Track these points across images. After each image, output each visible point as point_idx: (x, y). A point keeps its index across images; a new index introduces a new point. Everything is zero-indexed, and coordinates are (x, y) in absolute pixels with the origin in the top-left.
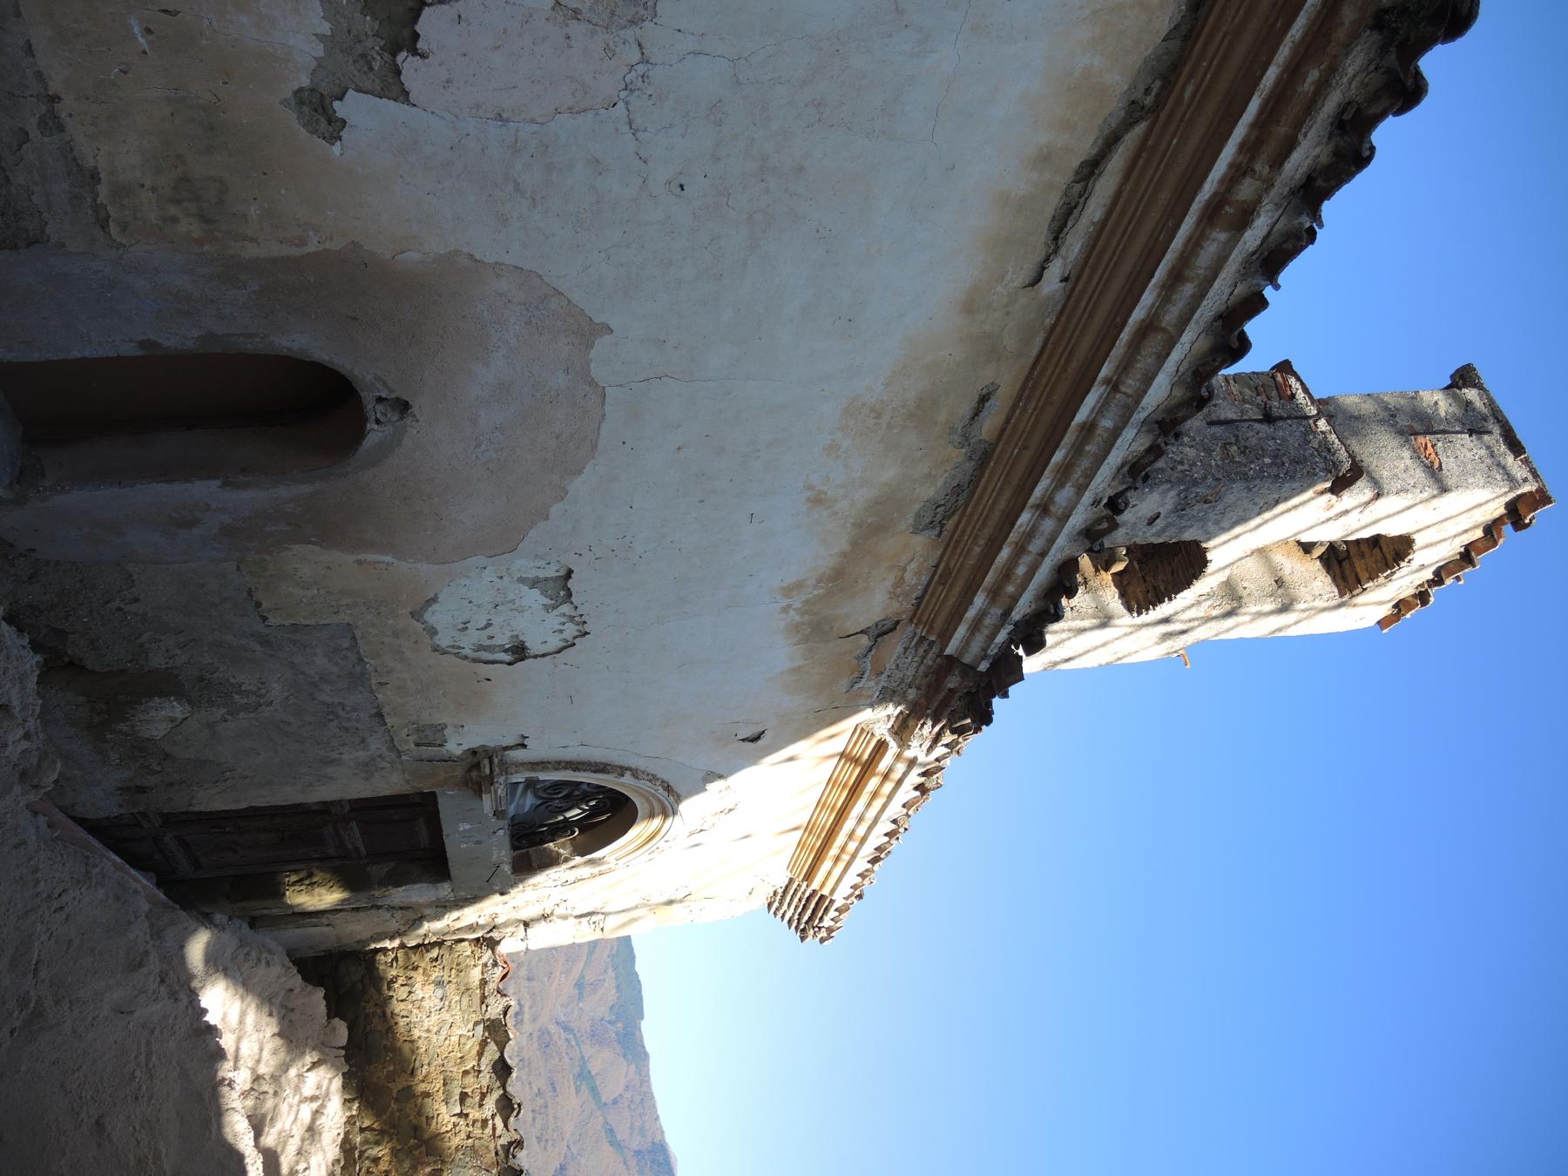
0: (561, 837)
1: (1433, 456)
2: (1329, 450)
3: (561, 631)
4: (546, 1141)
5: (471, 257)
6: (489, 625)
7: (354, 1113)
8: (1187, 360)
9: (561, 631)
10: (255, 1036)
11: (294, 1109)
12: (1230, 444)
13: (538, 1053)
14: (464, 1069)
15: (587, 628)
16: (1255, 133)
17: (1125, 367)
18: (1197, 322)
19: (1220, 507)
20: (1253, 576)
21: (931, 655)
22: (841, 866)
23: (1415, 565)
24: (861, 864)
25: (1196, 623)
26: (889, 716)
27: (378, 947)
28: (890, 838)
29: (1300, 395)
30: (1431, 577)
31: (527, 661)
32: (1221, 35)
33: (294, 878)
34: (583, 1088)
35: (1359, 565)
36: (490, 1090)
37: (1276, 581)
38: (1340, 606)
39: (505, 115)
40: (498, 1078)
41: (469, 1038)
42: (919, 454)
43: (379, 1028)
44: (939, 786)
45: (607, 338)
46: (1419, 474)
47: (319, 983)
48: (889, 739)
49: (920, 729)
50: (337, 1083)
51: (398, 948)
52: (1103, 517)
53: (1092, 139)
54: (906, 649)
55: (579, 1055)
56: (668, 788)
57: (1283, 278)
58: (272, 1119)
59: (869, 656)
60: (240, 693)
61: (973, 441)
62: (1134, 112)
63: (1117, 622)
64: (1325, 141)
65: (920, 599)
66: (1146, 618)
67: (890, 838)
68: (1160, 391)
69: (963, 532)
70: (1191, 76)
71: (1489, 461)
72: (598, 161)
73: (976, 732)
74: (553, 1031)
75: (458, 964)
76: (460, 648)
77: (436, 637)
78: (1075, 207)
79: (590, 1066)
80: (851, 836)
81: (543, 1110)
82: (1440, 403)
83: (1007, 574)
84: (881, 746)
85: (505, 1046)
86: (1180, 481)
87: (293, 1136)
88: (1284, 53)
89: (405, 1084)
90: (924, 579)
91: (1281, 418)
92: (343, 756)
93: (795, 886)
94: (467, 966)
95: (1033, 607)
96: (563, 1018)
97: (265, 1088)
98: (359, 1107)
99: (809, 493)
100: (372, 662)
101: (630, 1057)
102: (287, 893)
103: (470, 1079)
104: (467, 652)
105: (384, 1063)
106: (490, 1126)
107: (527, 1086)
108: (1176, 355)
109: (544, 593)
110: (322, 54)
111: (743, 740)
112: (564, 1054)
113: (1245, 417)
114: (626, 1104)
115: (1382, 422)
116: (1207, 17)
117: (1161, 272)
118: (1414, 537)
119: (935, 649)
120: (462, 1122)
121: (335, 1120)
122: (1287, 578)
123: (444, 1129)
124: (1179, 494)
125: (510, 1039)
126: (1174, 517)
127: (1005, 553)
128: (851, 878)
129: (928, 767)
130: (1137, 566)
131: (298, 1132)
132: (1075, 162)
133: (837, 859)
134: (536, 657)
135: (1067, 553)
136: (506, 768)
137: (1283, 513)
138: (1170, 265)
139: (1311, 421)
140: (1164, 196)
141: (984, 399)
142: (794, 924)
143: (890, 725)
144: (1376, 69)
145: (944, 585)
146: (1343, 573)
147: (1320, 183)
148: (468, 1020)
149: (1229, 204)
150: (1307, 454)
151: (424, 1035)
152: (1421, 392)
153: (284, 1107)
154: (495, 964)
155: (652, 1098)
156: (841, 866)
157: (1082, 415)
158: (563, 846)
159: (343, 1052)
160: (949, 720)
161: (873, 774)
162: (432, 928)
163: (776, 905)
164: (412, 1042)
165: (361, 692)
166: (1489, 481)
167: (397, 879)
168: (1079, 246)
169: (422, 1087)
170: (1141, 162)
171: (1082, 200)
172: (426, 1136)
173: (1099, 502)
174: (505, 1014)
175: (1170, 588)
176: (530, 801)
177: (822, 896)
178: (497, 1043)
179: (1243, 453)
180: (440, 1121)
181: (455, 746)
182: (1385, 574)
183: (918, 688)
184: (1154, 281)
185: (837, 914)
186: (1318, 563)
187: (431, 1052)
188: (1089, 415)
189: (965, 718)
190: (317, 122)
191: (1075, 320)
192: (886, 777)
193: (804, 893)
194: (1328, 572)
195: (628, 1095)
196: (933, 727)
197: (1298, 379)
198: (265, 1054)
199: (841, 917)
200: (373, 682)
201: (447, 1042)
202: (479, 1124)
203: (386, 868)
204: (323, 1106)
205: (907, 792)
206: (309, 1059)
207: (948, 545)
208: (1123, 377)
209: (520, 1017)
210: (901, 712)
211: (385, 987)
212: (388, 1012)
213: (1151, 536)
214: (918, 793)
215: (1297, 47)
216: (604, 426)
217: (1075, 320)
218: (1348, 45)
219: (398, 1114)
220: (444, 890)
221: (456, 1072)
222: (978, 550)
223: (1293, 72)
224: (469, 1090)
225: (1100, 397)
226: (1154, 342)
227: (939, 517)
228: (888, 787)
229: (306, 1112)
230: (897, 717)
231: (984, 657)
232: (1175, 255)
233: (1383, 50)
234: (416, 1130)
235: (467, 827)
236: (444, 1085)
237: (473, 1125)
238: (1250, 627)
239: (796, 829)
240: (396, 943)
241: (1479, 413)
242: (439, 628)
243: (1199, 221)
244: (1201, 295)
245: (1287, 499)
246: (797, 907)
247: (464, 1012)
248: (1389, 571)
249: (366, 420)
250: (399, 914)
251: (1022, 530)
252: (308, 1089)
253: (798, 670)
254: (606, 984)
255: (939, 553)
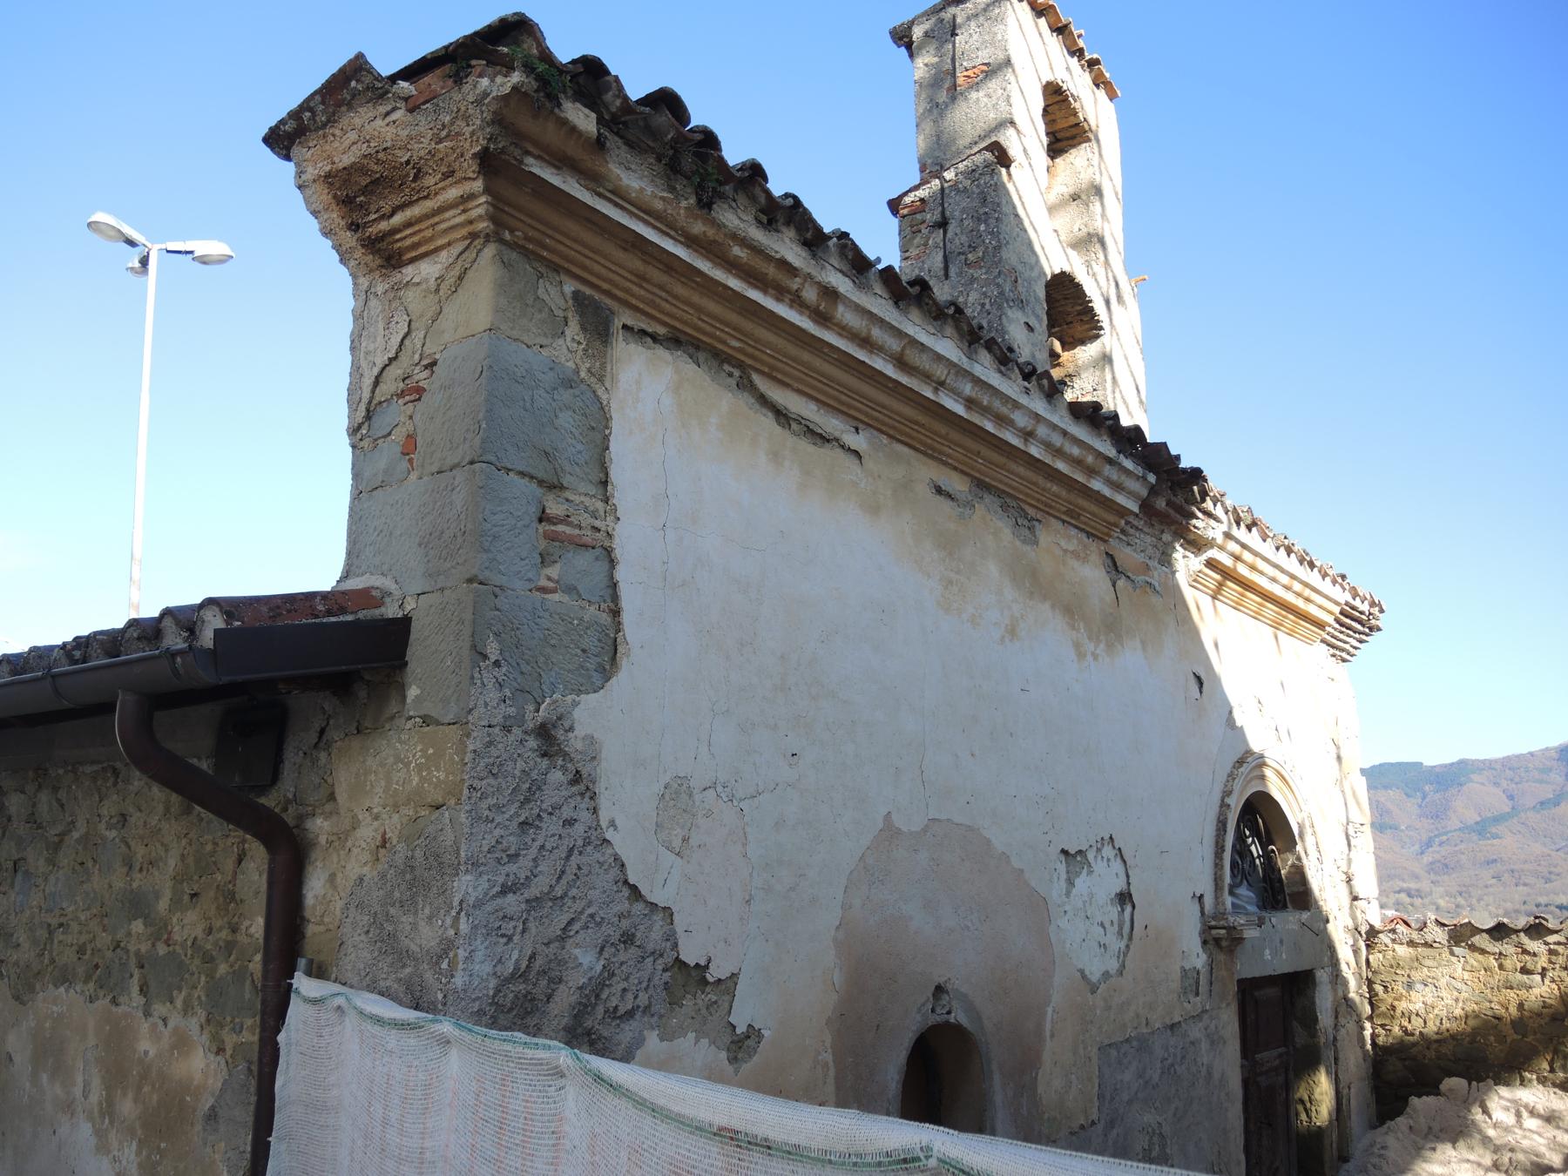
0: (1276, 863)
1: (975, 70)
2: (973, 171)
3: (1108, 860)
4: (1550, 873)
5: (837, 928)
6: (1102, 925)
7: (1534, 1077)
8: (926, 327)
9: (1108, 860)
10: (1454, 1166)
11: (1528, 1134)
12: (966, 260)
13: (1454, 875)
14: (1497, 969)
15: (1107, 837)
16: (770, 290)
17: (927, 377)
18: (900, 323)
19: (1020, 268)
20: (1072, 222)
21: (1136, 523)
22: (1314, 596)
23: (1066, 77)
24: (1313, 578)
25: (1110, 275)
26: (1184, 557)
27: (1369, 1042)
28: (1292, 552)
29: (921, 193)
30: (1076, 59)
31: (1132, 892)
32: (700, 323)
33: (1303, 1117)
34: (1494, 830)
35: (1062, 124)
36: (1519, 945)
37: (1074, 200)
38: (1098, 141)
39: (747, 898)
40: (1508, 936)
41: (1466, 962)
42: (978, 545)
43: (1451, 1047)
44: (1249, 510)
45: (894, 817)
46: (993, 84)
47: (1404, 1102)
48: (1204, 557)
49: (1199, 529)
50: (1503, 1091)
51: (1373, 1023)
52: (1038, 384)
53: (763, 418)
54: (1129, 544)
55: (1458, 833)
56: (1240, 762)
57: (872, 257)
58: (1537, 1156)
59: (1133, 577)
60: (1150, 1150)
61: (970, 498)
62: (745, 385)
63: (1108, 349)
64: (780, 235)
65: (1089, 535)
66: (1105, 324)
67: (1292, 552)
68: (948, 348)
69: (1038, 500)
70: (724, 342)
71: (981, 19)
72: (777, 823)
73: (1206, 481)
74: (1430, 859)
75: (1392, 967)
76: (1119, 952)
77: (1111, 972)
78: (808, 427)
79: (1471, 822)
80: (1288, 588)
81: (1516, 875)
82: (926, 61)
83: (1077, 463)
84: (1211, 564)
85: (1477, 928)
86: (1000, 307)
87: (1554, 1137)
88: (719, 274)
89: (1509, 1027)
90: (1074, 532)
91: (943, 213)
92: (1205, 1063)
93: (1329, 638)
94: (1394, 958)
95: (1105, 438)
96: (1417, 847)
97: (1506, 1160)
98: (1529, 1072)
99: (1007, 640)
100: (1129, 1030)
101: (1463, 779)
102: (1318, 1124)
103: (1508, 963)
104: (1122, 945)
105: (1487, 1045)
106: (1556, 947)
107: (1491, 890)
108: (923, 338)
109: (1078, 874)
110: (707, 1040)
111: (1201, 692)
112: (1457, 849)
113: (941, 245)
114: (1514, 786)
115: (941, 115)
116: (685, 333)
117: (861, 355)
118: (1044, 83)
119: (1131, 519)
120: (1550, 974)
121: (1541, 1096)
122: (1071, 190)
123: (1556, 992)
124: (1011, 307)
125: (1470, 923)
126: (1028, 310)
127: (1061, 466)
128: (1326, 586)
129: (1233, 521)
130: (1056, 329)
131: (1550, 1132)
132: (778, 429)
133: (1308, 600)
134: (1129, 884)
135: (1065, 412)
136: (1220, 914)
137: (1025, 209)
138: (857, 348)
139: (946, 185)
140: (806, 356)
141: (939, 491)
142: (1364, 637)
143: (1192, 556)
144: (735, 201)
145: (1079, 515)
146: (1068, 139)
147: (809, 235)
148: (1447, 961)
149: (818, 307)
150: (977, 191)
151: (1460, 1004)
152: (916, 78)
153: (1525, 1143)
154: (1393, 931)
155: (1508, 758)
156: (1314, 596)
157: (959, 409)
158: (1285, 861)
159: (1474, 1083)
160: (1193, 504)
161: (1235, 569)
162: (1355, 989)
163: (1344, 655)
164: (1467, 1017)
165: (1153, 1043)
166: (1000, 19)
167: (1310, 1020)
168: (834, 421)
169: (1513, 1010)
170: (779, 376)
171: (803, 421)
172: (1562, 1009)
173: (1027, 388)
174: (1444, 925)
175: (1080, 301)
176: (1243, 891)
177: (1341, 613)
178: (1473, 935)
179: (975, 248)
180: (1547, 995)
181: (1198, 959)
182: (1072, 102)
183: (1163, 532)
184: (867, 361)
185: (1358, 598)
186: (1057, 160)
187: (1478, 999)
188: (961, 403)
189: (1193, 491)
190: (748, 1047)
191: (886, 419)
192: (1237, 558)
193: (1335, 629)
194: (1066, 152)
195: (1504, 784)
196: (1197, 518)
197: (906, 194)
198: (1472, 1157)
199: (1361, 594)
200: (1145, 1031)
201: (1469, 983)
202: (1554, 958)
203: (1297, 1027)
204: (1526, 1107)
205: (1252, 539)
206: (1477, 1114)
207: (1048, 513)
208: (935, 379)
209: (1413, 892)
210: (1181, 545)
211: (1411, 1038)
212: (1436, 1037)
213: (1041, 325)
214: (1254, 529)
215: (716, 264)
216: (956, 821)
217: (886, 419)
218: (719, 225)
219: (1538, 1036)
220: (1322, 976)
221: (1499, 976)
222: (1055, 488)
223: (732, 266)
224: (1519, 966)
225: (947, 395)
226: (914, 357)
227: (1026, 522)
228: (1247, 556)
229: (1531, 1123)
230: (1185, 549)
231: (1144, 478)
232: (849, 344)
233: (722, 197)
234: (1556, 1018)
235: (1267, 952)
236: (1512, 988)
237: (1554, 964)
238: (1111, 219)
239: (1276, 638)
240: (1368, 1025)
241: (936, 26)
242: (1103, 969)
243: (828, 328)
244: (882, 322)
245: (1014, 207)
246: (1348, 636)
247: (1440, 965)
248: (1070, 99)
249: (947, 1023)
250: (1342, 1021)
251: (1043, 452)
252: (1508, 1119)
253: (1143, 643)
254: (1383, 799)
255: (1053, 520)
